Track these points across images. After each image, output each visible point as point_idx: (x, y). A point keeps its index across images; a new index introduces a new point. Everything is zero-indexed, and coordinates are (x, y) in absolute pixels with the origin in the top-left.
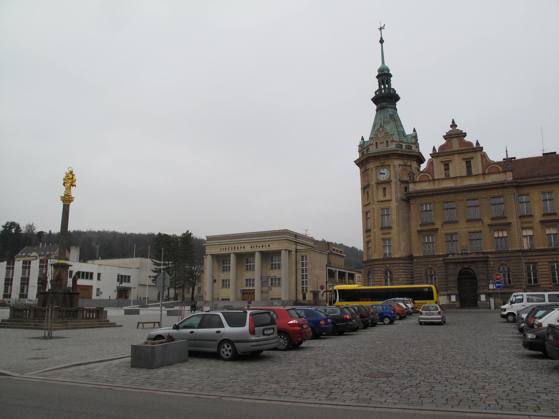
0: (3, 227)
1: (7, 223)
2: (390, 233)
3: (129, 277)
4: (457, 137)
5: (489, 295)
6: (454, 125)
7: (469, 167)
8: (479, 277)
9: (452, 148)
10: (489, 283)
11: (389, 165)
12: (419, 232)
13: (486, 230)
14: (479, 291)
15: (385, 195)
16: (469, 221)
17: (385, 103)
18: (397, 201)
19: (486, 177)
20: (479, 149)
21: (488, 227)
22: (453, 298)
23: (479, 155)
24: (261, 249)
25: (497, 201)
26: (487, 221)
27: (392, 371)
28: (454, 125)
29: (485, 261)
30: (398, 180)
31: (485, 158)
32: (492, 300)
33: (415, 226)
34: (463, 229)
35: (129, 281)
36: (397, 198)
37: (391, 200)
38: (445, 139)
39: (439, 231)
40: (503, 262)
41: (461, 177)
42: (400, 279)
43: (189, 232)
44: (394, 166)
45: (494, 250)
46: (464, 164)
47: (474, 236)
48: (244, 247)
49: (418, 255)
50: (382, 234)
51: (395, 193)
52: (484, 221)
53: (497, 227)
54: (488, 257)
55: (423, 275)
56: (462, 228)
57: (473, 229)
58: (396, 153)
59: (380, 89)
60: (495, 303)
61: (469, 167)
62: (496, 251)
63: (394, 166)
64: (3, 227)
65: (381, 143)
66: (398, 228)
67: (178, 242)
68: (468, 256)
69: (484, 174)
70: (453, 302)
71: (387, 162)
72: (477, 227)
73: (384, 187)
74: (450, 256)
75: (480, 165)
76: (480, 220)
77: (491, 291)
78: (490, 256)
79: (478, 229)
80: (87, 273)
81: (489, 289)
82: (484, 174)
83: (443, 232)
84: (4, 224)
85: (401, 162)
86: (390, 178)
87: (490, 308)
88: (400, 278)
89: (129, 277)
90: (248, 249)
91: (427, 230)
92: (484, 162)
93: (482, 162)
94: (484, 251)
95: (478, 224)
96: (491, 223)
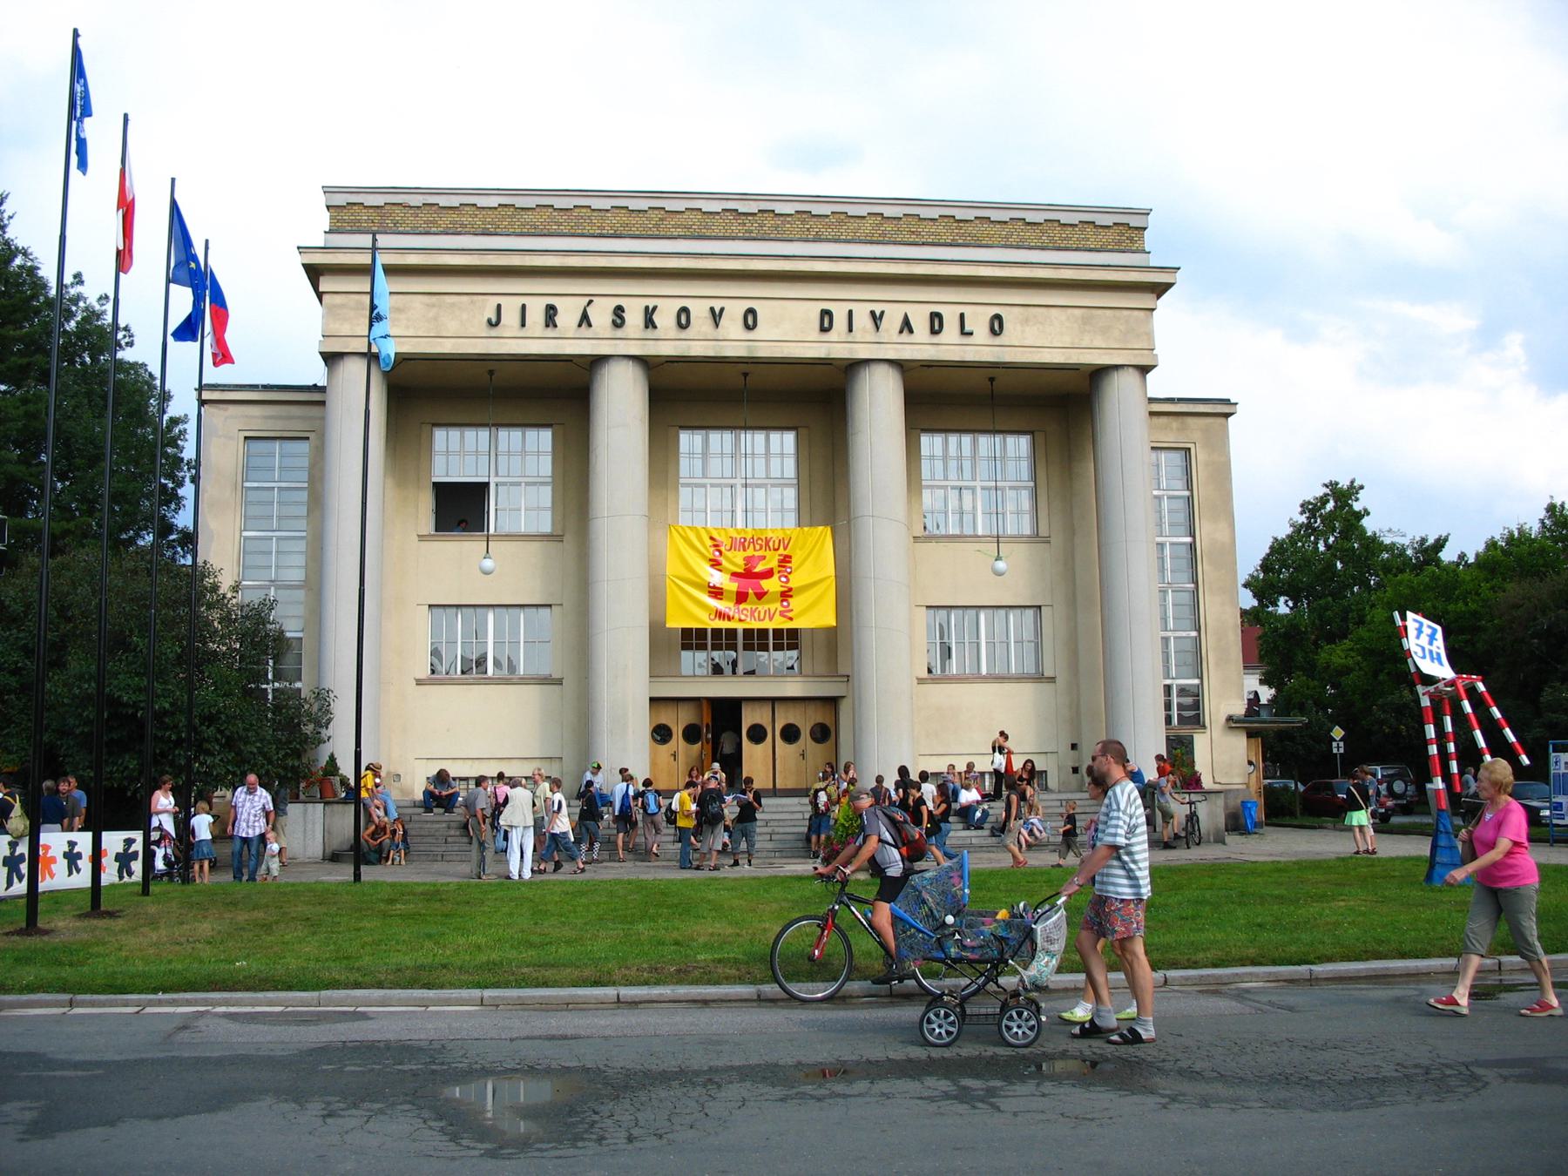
24: (921, 347)
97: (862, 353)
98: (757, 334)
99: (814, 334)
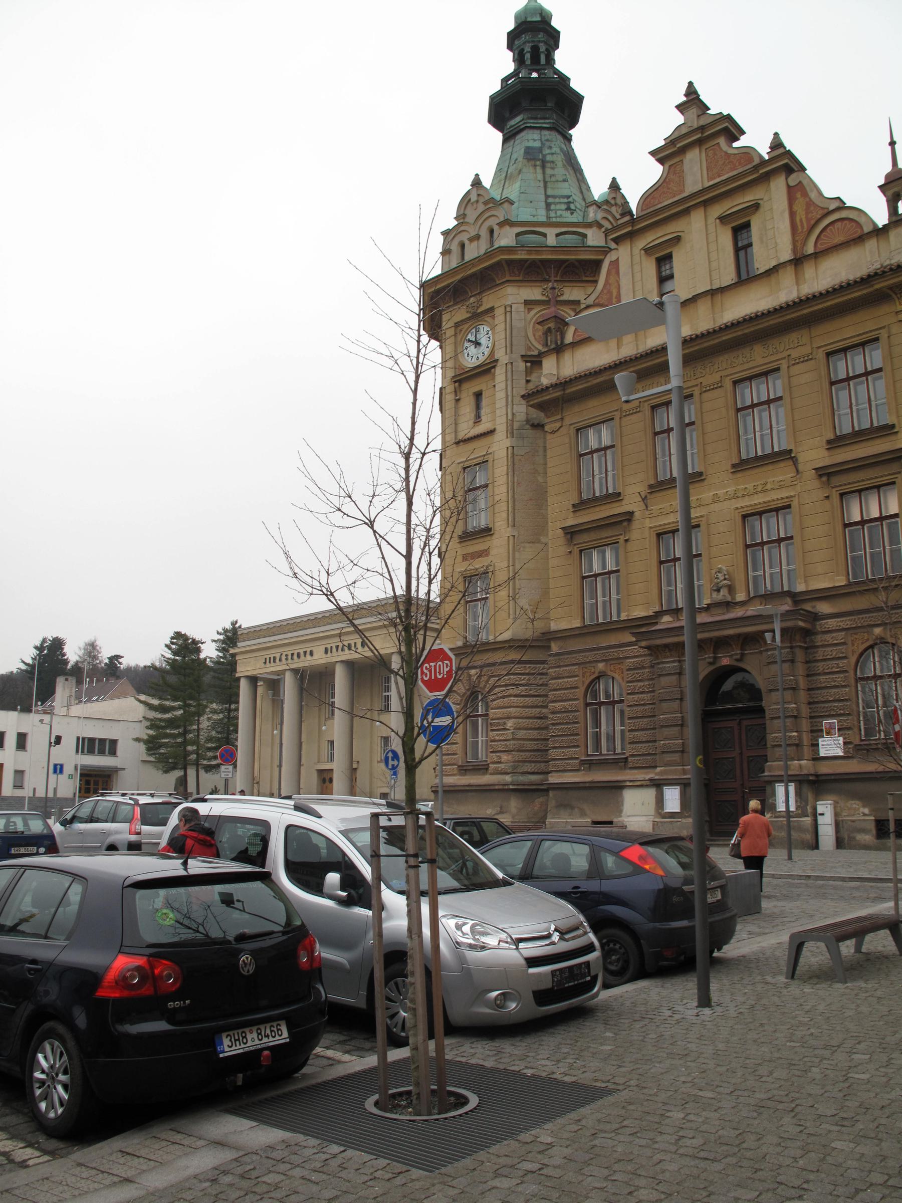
0: (36, 648)
1: (44, 641)
2: (485, 553)
3: (114, 742)
4: (700, 142)
5: (815, 784)
6: (692, 100)
7: (742, 249)
8: (772, 703)
9: (683, 191)
10: (816, 733)
11: (492, 309)
12: (571, 533)
13: (809, 494)
14: (774, 767)
15: (478, 419)
16: (742, 466)
17: (518, 119)
18: (511, 433)
19: (809, 270)
20: (784, 163)
21: (816, 483)
22: (673, 799)
23: (778, 187)
25: (857, 362)
26: (814, 454)
27: (594, 1075)
28: (692, 100)
29: (803, 633)
30: (516, 356)
31: (805, 194)
32: (826, 809)
33: (560, 513)
34: (721, 501)
35: (113, 752)
36: (510, 423)
37: (491, 432)
38: (661, 161)
39: (636, 524)
40: (877, 631)
41: (712, 293)
42: (510, 724)
43: (221, 630)
44: (508, 310)
45: (841, 581)
46: (726, 238)
47: (768, 528)
48: (311, 653)
49: (564, 625)
50: (465, 558)
51: (502, 404)
52: (801, 458)
53: (861, 475)
54: (816, 617)
55: (579, 703)
56: (716, 500)
57: (758, 500)
58: (510, 262)
59: (515, 74)
60: (837, 825)
61: (742, 249)
62: (850, 584)
63: (508, 310)
64: (36, 648)
65: (471, 240)
66: (509, 532)
67: (482, 700)
68: (738, 613)
69: (798, 261)
70: (672, 815)
71: (488, 301)
72: (773, 484)
73: (476, 389)
74: (666, 618)
75: (784, 225)
76: (786, 455)
77: (825, 769)
78: (824, 608)
79: (776, 496)
80: (102, 741)
81: (817, 759)
82: (798, 261)
83: (648, 523)
84: (38, 644)
85: (534, 293)
86: (492, 353)
87: (816, 846)
88: (508, 718)
89: (114, 742)
90: (319, 658)
91: (598, 526)
92: (800, 208)
93: (792, 214)
94: (800, 587)
95: (782, 473)
96: (827, 462)
97: (334, 659)
98: (315, 656)
99: (324, 656)
